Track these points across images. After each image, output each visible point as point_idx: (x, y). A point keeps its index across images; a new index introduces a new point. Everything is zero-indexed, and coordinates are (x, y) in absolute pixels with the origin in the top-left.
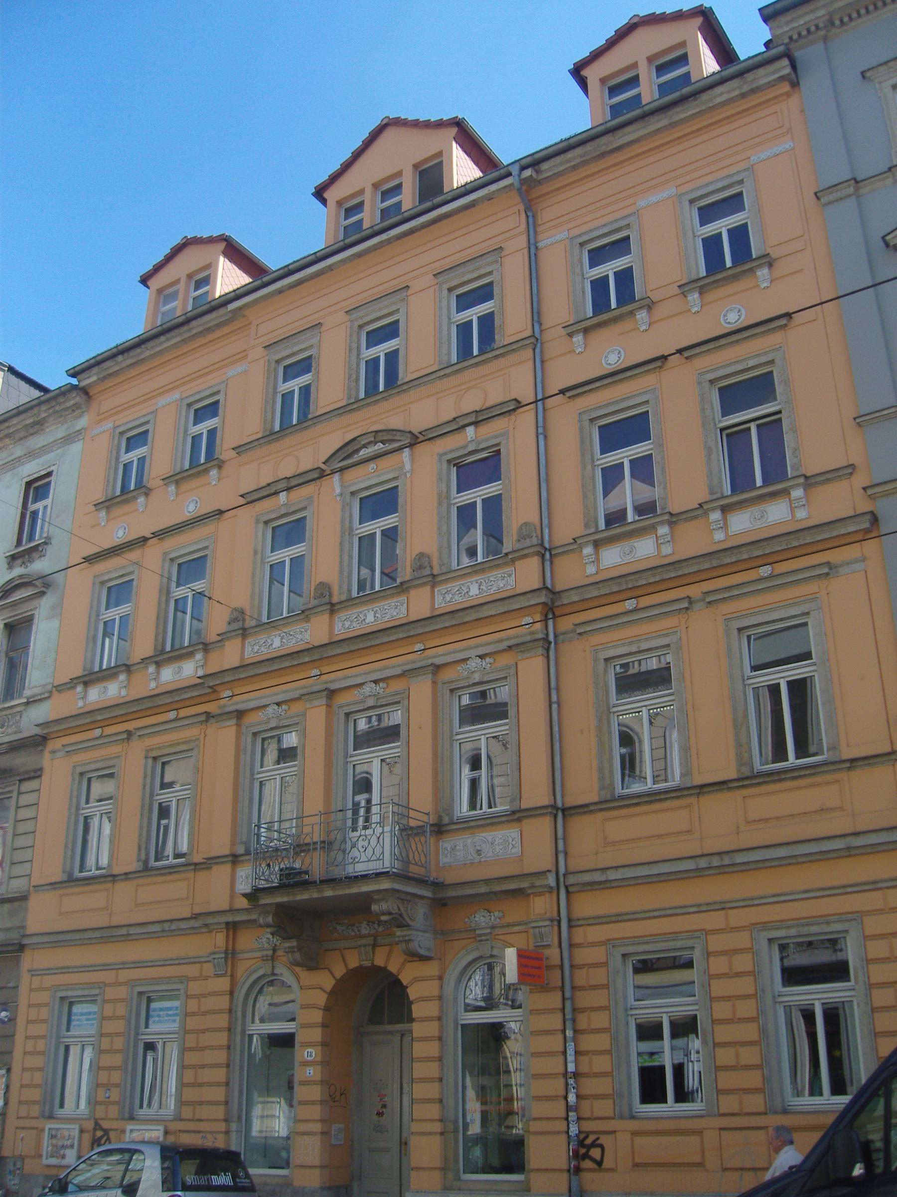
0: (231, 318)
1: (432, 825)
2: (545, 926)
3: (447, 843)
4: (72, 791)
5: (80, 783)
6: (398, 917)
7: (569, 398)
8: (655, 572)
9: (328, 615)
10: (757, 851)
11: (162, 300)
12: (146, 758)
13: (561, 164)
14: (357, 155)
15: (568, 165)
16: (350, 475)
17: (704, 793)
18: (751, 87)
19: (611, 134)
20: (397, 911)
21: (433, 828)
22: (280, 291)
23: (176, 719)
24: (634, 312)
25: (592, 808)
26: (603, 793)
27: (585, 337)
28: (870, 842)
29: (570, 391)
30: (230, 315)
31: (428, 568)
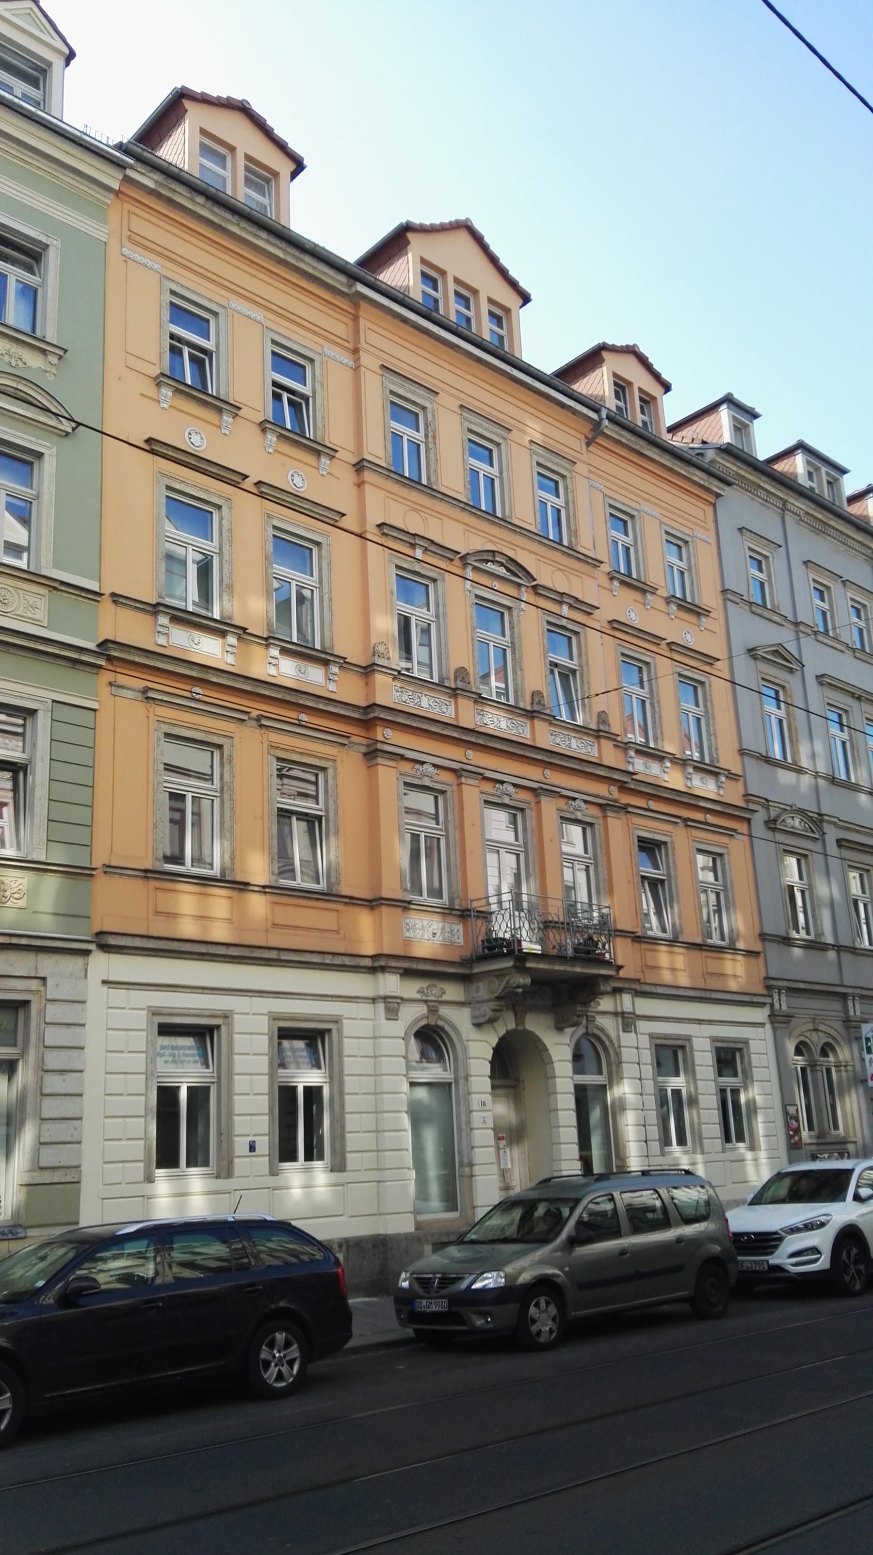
13: (617, 433)
22: (405, 320)
28: (263, 956)
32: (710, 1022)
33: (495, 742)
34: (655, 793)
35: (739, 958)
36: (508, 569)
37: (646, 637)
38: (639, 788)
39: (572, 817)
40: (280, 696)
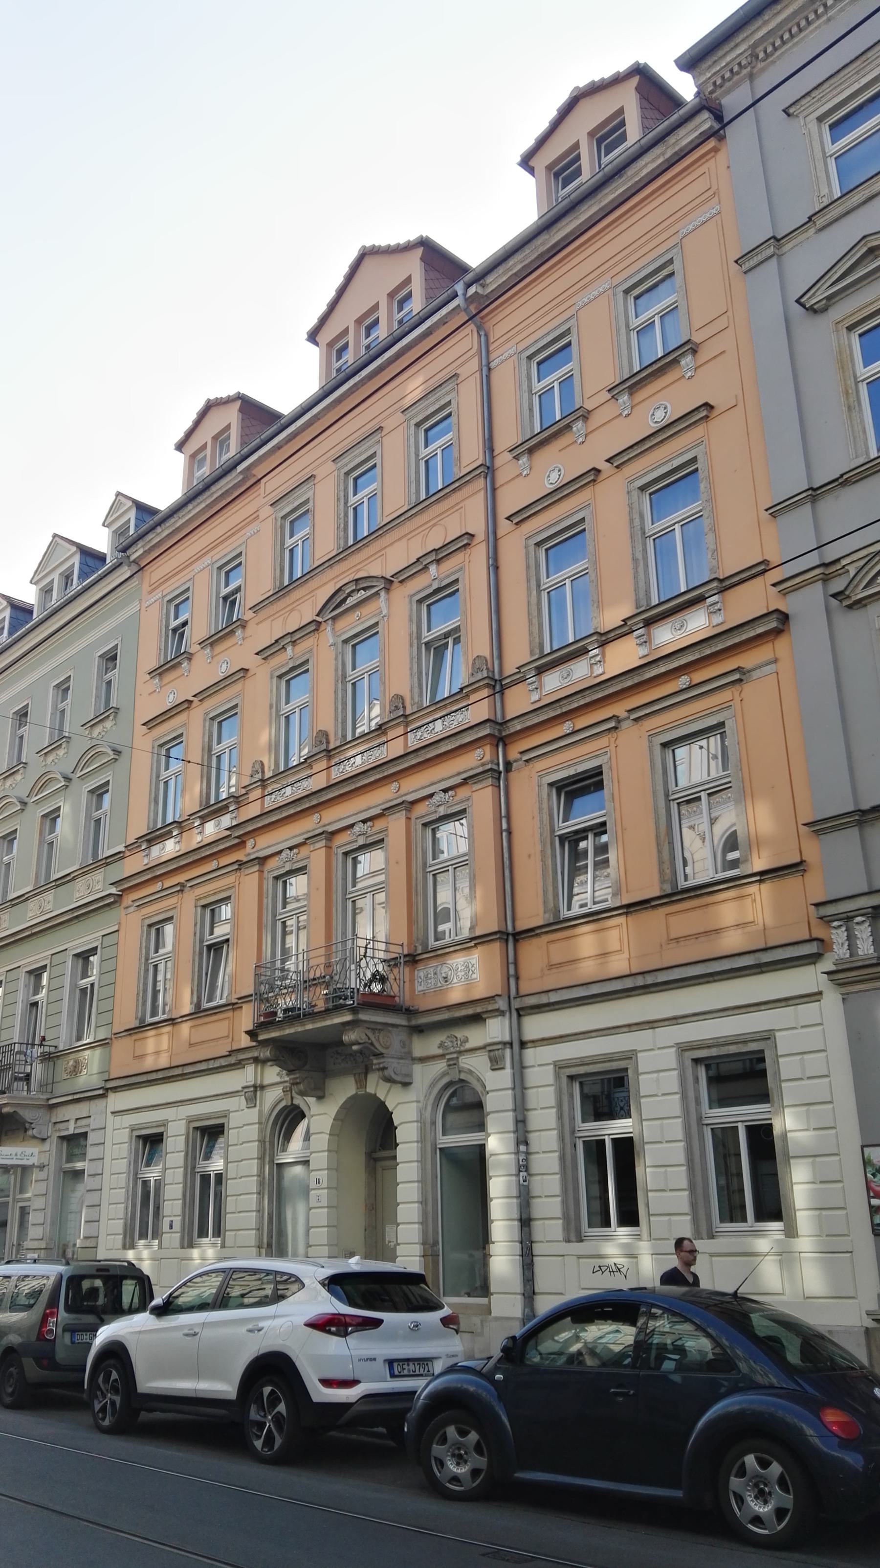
0: (243, 479)
1: (405, 956)
2: (498, 1050)
3: (421, 972)
4: (141, 943)
5: (149, 934)
6: (370, 1046)
7: (517, 524)
8: (584, 694)
9: (325, 761)
10: (676, 970)
11: (196, 466)
12: (196, 907)
13: (504, 273)
14: (341, 292)
15: (510, 273)
16: (341, 624)
17: (631, 912)
18: (674, 151)
19: (546, 231)
20: (367, 1040)
21: (407, 959)
23: (574, 733)
24: (570, 424)
25: (538, 931)
26: (547, 915)
27: (530, 459)
29: (519, 517)
30: (241, 477)
31: (402, 709)
32: (675, 1020)
33: (327, 794)
34: (559, 712)
35: (753, 889)
36: (364, 589)
37: (566, 492)
38: (529, 723)
39: (437, 816)
40: (191, 860)
